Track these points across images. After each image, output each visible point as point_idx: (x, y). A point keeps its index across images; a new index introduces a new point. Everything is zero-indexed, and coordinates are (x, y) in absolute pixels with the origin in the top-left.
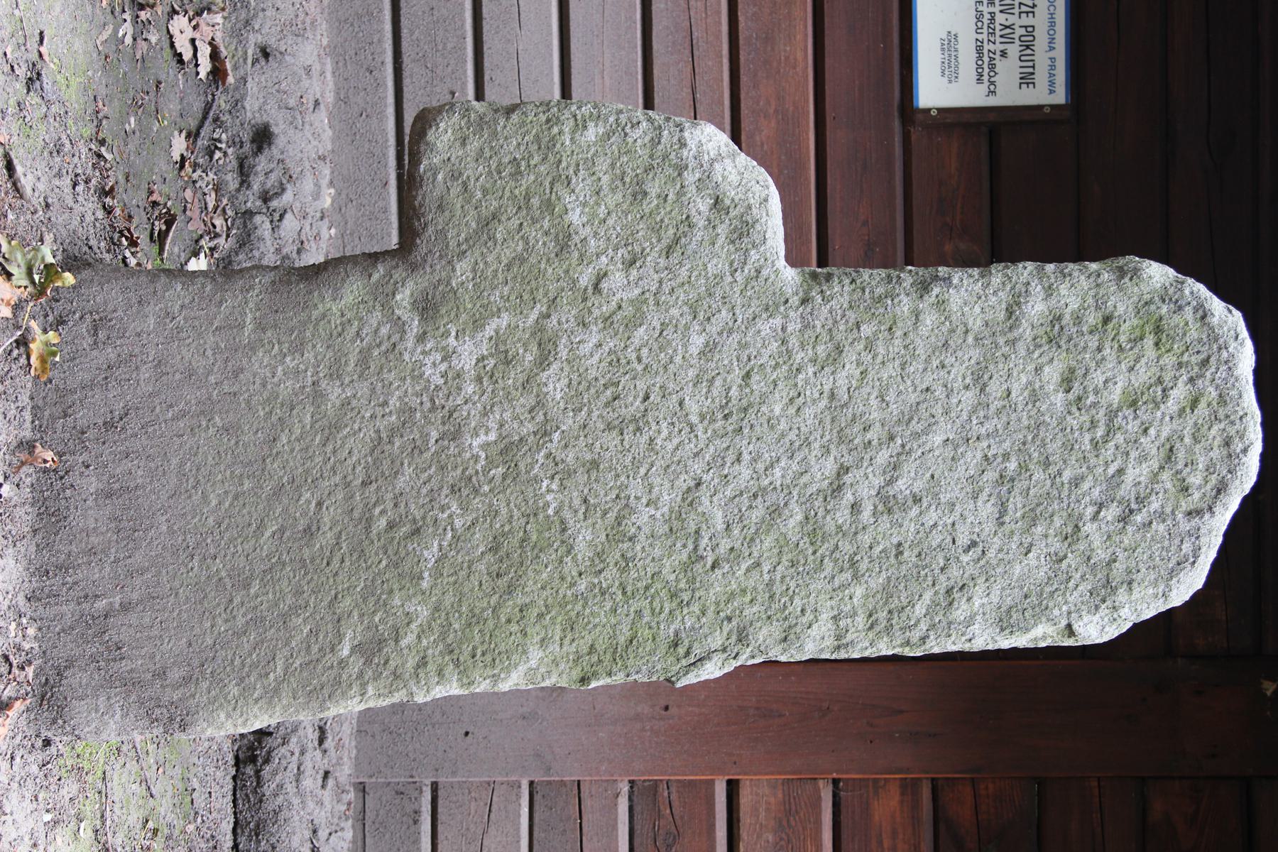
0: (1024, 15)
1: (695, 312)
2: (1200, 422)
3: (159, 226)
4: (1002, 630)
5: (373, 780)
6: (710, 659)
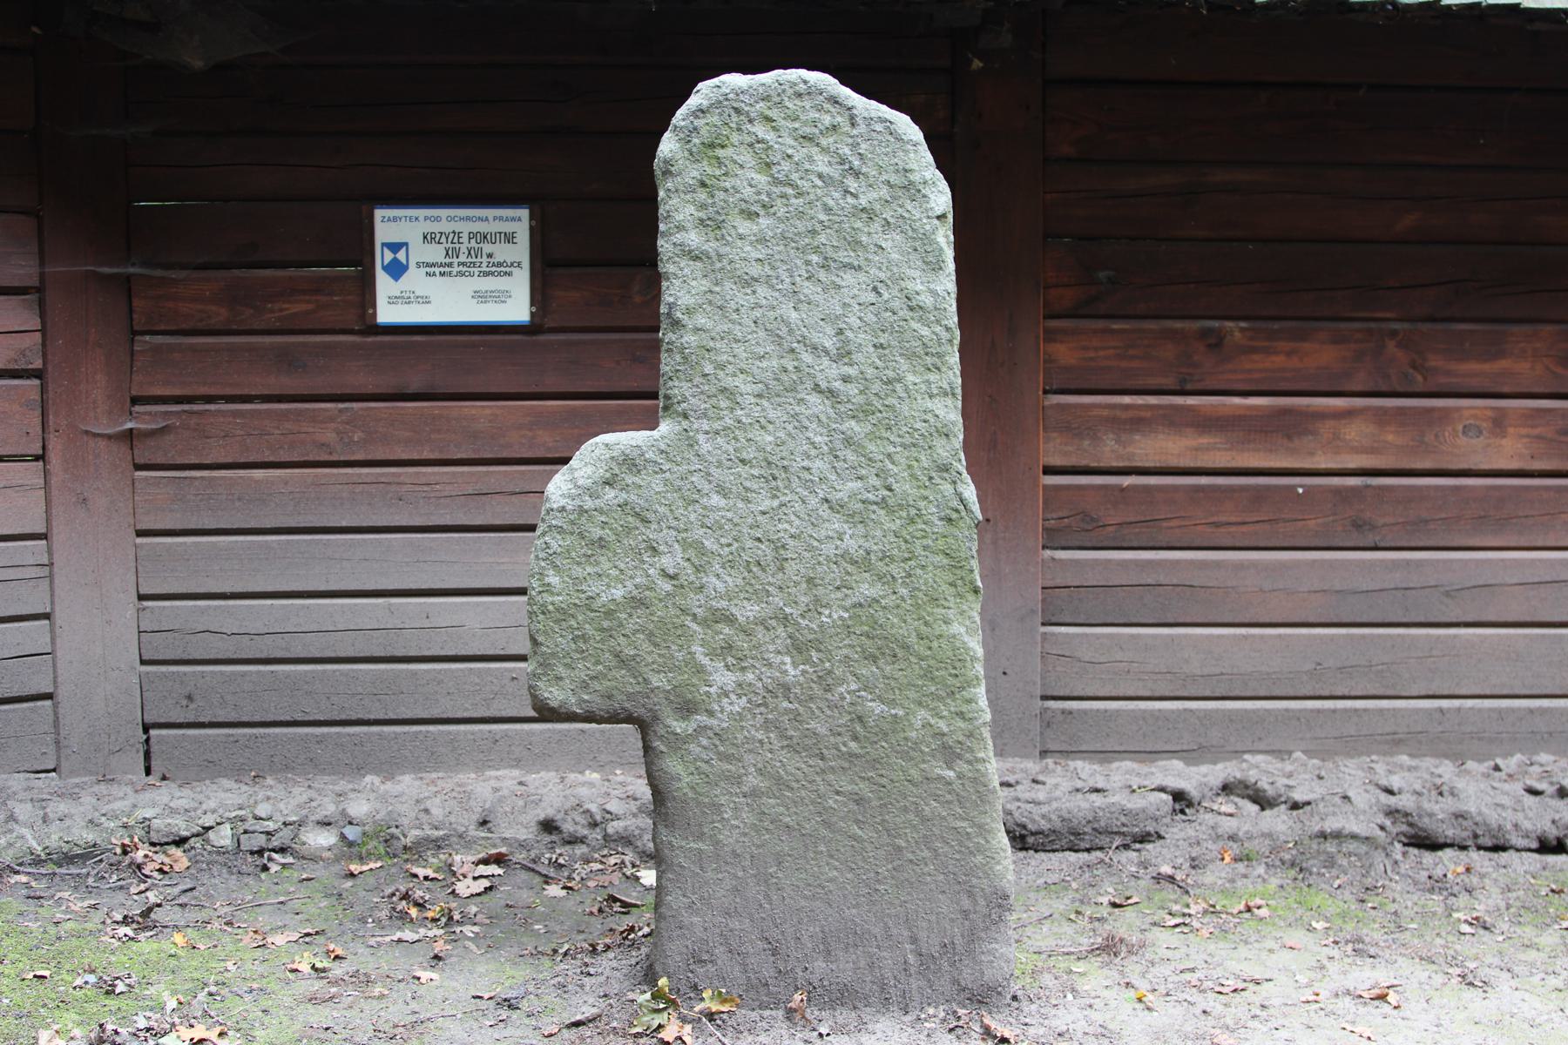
0: (461, 240)
1: (693, 501)
2: (783, 115)
3: (617, 907)
4: (941, 268)
5: (1038, 745)
6: (961, 494)
